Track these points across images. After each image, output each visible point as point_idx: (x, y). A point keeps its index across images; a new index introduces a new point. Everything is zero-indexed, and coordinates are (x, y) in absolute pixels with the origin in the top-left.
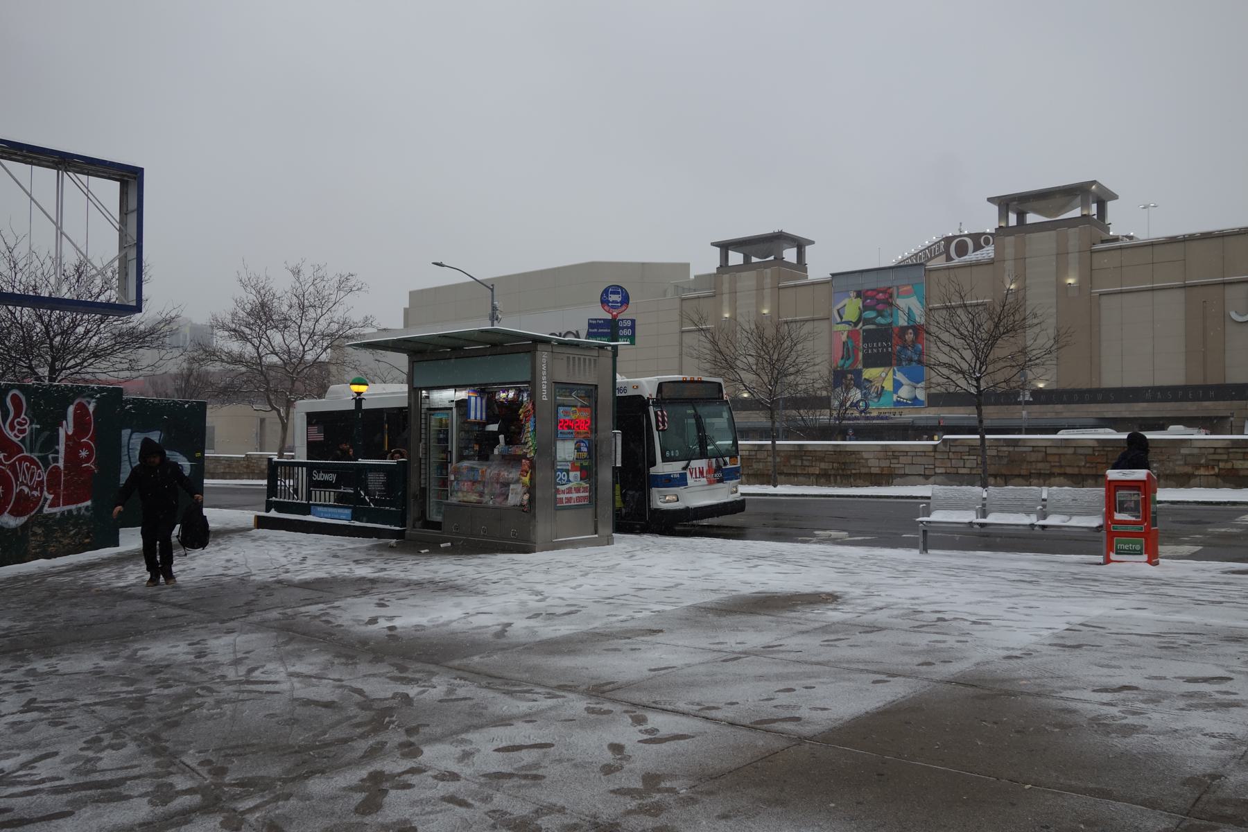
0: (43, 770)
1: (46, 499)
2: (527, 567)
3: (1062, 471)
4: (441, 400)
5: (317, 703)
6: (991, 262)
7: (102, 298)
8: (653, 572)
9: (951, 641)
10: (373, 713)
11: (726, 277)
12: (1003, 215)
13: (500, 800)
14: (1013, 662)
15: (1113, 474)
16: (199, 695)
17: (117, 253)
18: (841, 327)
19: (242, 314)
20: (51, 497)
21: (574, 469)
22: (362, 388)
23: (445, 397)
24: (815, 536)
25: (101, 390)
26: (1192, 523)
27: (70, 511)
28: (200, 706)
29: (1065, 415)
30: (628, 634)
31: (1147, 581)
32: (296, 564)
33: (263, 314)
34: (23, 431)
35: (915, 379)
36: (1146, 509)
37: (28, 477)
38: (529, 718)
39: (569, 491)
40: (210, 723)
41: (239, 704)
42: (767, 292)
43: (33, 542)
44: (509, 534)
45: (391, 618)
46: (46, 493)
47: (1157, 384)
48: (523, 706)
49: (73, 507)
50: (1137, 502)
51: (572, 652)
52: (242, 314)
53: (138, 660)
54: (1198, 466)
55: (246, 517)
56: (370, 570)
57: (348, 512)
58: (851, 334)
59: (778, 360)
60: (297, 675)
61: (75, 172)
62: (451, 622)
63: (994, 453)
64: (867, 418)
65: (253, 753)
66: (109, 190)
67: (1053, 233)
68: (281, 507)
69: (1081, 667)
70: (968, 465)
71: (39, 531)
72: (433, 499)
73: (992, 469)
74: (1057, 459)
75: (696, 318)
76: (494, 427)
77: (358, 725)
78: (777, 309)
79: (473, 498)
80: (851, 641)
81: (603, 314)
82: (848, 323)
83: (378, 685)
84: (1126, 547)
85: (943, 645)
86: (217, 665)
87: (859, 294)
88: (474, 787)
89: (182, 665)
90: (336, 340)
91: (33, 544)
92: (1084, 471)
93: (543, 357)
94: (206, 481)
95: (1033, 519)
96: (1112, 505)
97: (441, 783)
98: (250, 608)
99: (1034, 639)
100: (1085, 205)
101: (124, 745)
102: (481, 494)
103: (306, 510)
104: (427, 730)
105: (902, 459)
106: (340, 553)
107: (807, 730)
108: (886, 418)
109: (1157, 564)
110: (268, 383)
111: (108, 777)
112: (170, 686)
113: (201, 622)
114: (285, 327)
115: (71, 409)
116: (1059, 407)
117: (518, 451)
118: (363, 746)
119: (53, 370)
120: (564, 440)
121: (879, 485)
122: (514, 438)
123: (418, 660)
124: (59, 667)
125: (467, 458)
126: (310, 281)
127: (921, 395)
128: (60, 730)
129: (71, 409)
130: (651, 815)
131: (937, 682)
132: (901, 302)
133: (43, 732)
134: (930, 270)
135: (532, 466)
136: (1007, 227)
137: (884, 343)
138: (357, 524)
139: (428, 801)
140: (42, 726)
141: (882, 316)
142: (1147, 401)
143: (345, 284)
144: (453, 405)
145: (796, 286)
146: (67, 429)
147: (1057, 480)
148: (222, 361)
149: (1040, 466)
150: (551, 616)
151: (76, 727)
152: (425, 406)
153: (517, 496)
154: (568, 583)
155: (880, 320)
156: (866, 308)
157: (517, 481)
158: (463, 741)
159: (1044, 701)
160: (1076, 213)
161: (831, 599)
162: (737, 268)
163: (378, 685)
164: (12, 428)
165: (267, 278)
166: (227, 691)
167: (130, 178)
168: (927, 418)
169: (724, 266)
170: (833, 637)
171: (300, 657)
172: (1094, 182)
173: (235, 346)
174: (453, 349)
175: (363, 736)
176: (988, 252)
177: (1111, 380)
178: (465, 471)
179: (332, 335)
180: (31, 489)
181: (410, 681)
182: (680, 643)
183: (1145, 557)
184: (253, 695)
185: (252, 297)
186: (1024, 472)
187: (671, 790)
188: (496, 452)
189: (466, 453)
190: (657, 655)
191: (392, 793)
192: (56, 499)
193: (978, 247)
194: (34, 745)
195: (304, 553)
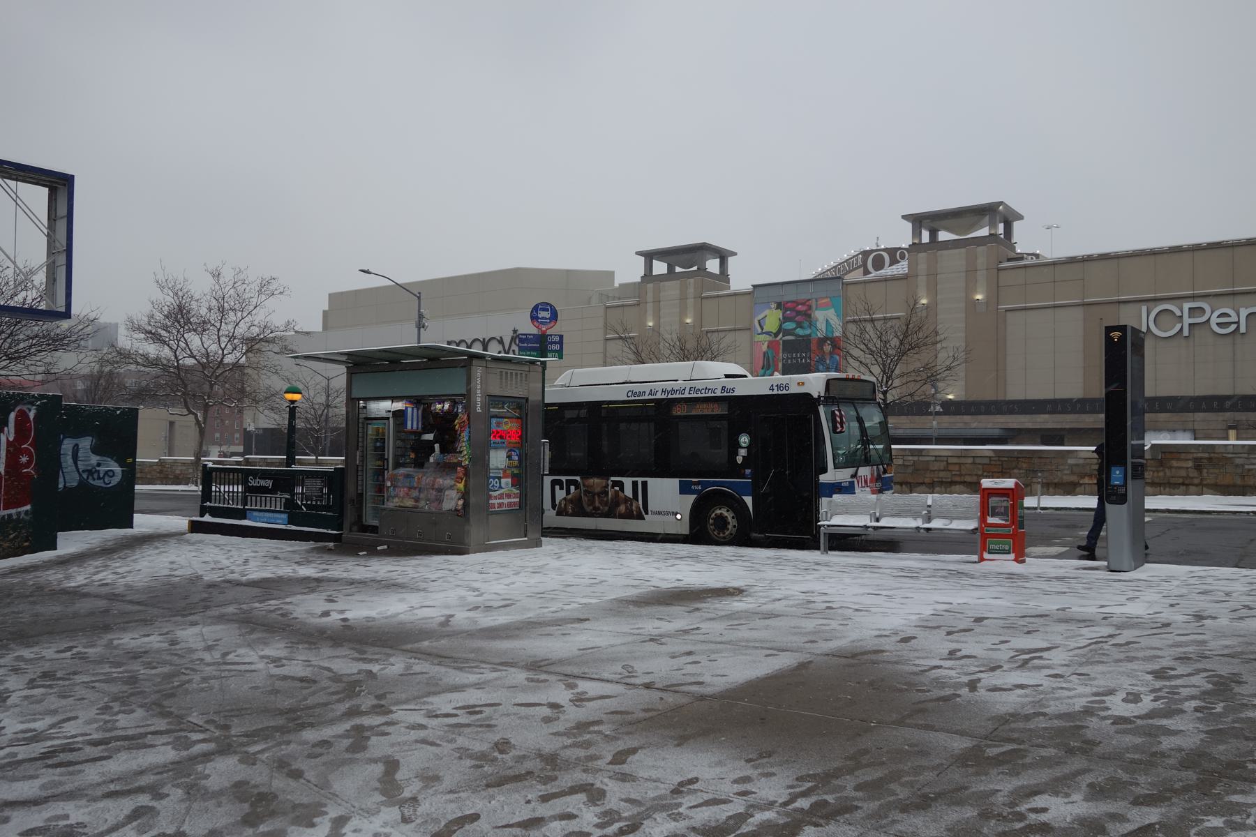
0: (71, 728)
2: (463, 567)
4: (379, 410)
5: (293, 678)
6: (905, 278)
8: (578, 571)
9: (834, 624)
11: (650, 286)
12: (917, 233)
13: (461, 741)
14: (882, 639)
15: (987, 483)
18: (762, 337)
19: (159, 316)
21: (505, 477)
22: (297, 397)
23: (382, 407)
25: (42, 397)
26: (1067, 527)
27: (10, 516)
28: (189, 681)
29: (974, 425)
30: (559, 622)
31: (1011, 576)
33: (181, 316)
38: (478, 686)
39: (501, 497)
40: (203, 694)
42: (690, 302)
44: (442, 537)
45: (342, 612)
47: (1058, 396)
48: (472, 678)
49: (13, 511)
50: (1006, 508)
51: (508, 637)
52: (159, 316)
53: (116, 648)
54: (1083, 476)
55: (180, 523)
57: (285, 516)
58: (771, 345)
60: (268, 657)
63: (900, 462)
66: (38, 196)
67: (963, 250)
68: (215, 512)
72: (369, 506)
74: (957, 468)
75: (620, 329)
76: (429, 437)
77: (333, 693)
78: (700, 318)
79: (409, 503)
80: (750, 626)
81: (529, 328)
82: (767, 333)
83: (345, 664)
86: (191, 651)
87: (779, 306)
89: (158, 651)
90: (252, 344)
93: (478, 371)
94: (137, 487)
95: (919, 523)
96: (985, 511)
98: (206, 605)
99: (904, 622)
100: (993, 225)
101: (133, 711)
102: (417, 500)
103: (242, 514)
104: (392, 696)
107: (708, 690)
109: (1024, 561)
110: (185, 386)
111: (130, 732)
115: (12, 416)
116: (967, 418)
117: (452, 459)
118: (342, 708)
120: (496, 448)
122: (449, 445)
123: (373, 645)
124: (44, 654)
125: (403, 465)
126: (231, 283)
129: (12, 416)
133: (53, 702)
134: (848, 284)
135: (467, 474)
136: (920, 243)
138: (294, 528)
139: (405, 743)
140: (53, 698)
141: (802, 327)
143: (265, 287)
144: (390, 415)
145: (718, 296)
147: (958, 487)
148: (138, 364)
149: (942, 474)
150: (489, 608)
152: (362, 416)
153: (452, 501)
155: (800, 331)
156: (786, 319)
157: (451, 488)
158: (424, 703)
159: (899, 667)
160: (984, 232)
161: (738, 592)
162: (661, 278)
163: (345, 664)
165: (185, 280)
166: (209, 670)
167: (59, 185)
169: (648, 275)
171: (266, 644)
172: (1001, 203)
173: (152, 349)
174: (391, 362)
175: (339, 701)
176: (902, 268)
177: (1016, 391)
181: (370, 661)
182: (605, 628)
183: (1012, 556)
186: (927, 480)
187: (599, 732)
188: (431, 460)
191: (374, 739)
193: (894, 262)
194: (54, 712)
195: (245, 556)
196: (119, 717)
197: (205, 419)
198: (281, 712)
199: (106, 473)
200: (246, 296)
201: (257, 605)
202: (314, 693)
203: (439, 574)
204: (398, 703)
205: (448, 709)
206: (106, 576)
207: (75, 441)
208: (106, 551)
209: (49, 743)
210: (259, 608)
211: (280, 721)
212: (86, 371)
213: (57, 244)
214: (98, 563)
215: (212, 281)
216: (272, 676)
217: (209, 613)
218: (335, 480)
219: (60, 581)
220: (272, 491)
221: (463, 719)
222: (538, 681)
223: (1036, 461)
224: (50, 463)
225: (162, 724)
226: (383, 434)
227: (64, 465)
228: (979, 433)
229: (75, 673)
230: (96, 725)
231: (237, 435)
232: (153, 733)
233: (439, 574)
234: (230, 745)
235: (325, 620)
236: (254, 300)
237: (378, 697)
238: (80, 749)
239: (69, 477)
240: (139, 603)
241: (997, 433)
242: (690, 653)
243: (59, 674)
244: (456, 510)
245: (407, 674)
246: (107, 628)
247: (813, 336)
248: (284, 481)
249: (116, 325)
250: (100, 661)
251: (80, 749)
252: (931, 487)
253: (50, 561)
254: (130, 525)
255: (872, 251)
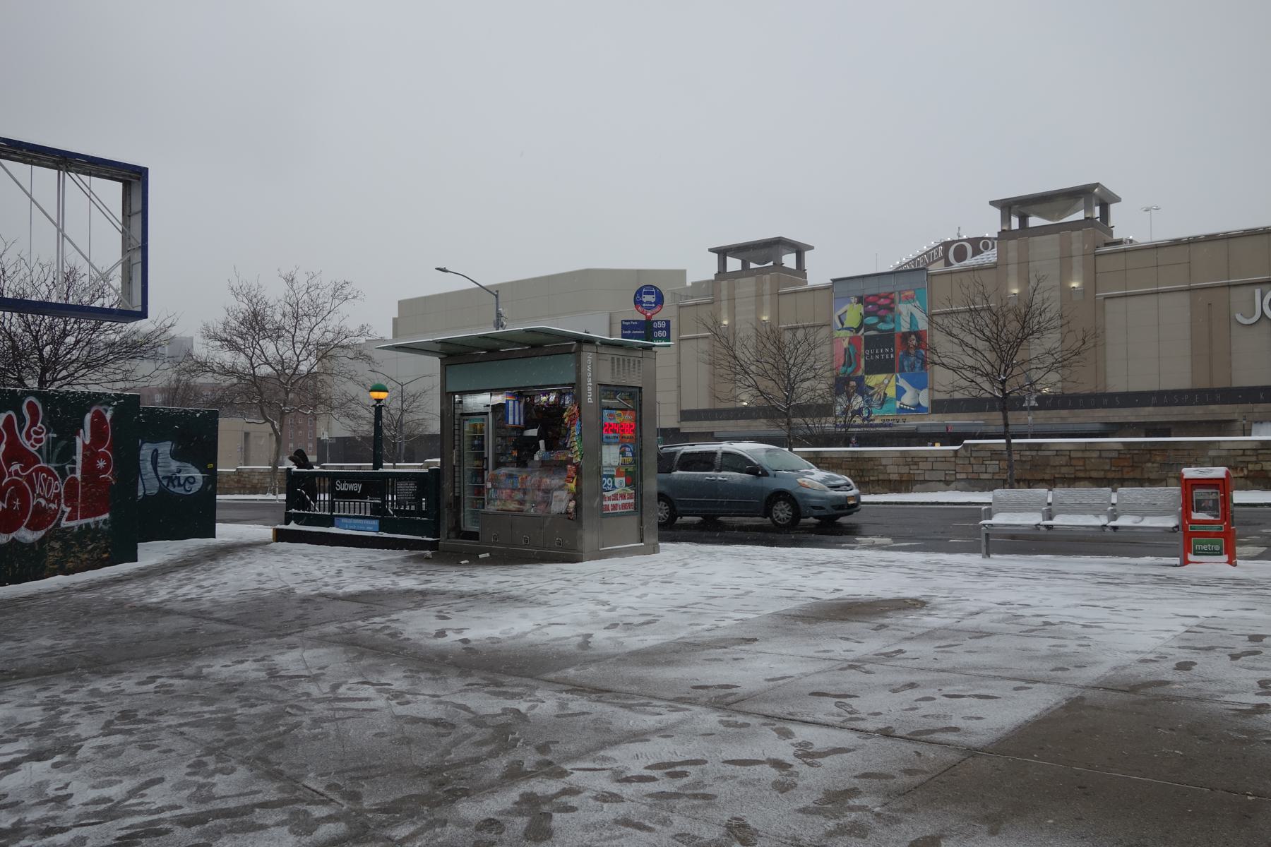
0: (156, 797)
1: (63, 512)
3: (1087, 475)
4: (476, 405)
5: (424, 720)
6: (994, 266)
7: (97, 304)
9: (1072, 646)
10: (491, 730)
12: (1006, 219)
15: (1190, 473)
16: (291, 714)
17: (119, 256)
18: (843, 333)
19: (234, 324)
20: (68, 510)
21: (619, 475)
22: (383, 395)
24: (857, 542)
25: (119, 397)
27: (88, 525)
29: (1071, 420)
30: (723, 643)
32: (332, 577)
34: (39, 441)
35: (919, 386)
36: (1225, 509)
37: (45, 489)
38: (664, 732)
39: (615, 497)
40: (317, 744)
41: (340, 722)
42: (767, 298)
43: (51, 558)
44: (556, 543)
45: (459, 631)
46: (63, 506)
47: (1163, 388)
48: (647, 721)
49: (91, 520)
50: (1215, 501)
51: (669, 663)
52: (234, 324)
53: (206, 678)
56: (414, 582)
57: (376, 523)
58: (852, 341)
59: (794, 365)
61: (77, 172)
62: (526, 633)
64: (872, 426)
65: (381, 775)
66: (111, 191)
68: (299, 519)
69: (1215, 668)
70: (990, 470)
71: (57, 545)
72: (467, 509)
73: (1017, 473)
76: (533, 432)
78: (776, 315)
79: (513, 506)
82: (849, 329)
84: (1204, 547)
85: (1066, 650)
87: (860, 300)
88: (645, 808)
89: (256, 682)
90: (325, 352)
91: (51, 559)
92: (1110, 475)
93: (588, 357)
95: (1103, 520)
96: (1188, 505)
97: (605, 805)
98: (303, 624)
99: (1159, 642)
100: (1088, 208)
101: (233, 770)
103: (329, 521)
105: (922, 465)
106: (375, 566)
107: (973, 741)
108: (890, 425)
110: (261, 395)
111: (232, 804)
112: (252, 706)
113: (258, 638)
114: (279, 337)
115: (88, 417)
116: (1064, 413)
117: (561, 456)
118: (499, 766)
119: (42, 382)
120: (608, 444)
121: (899, 491)
124: (123, 686)
126: (304, 289)
127: (925, 402)
128: (154, 753)
129: (88, 417)
130: (856, 836)
131: (1082, 687)
132: (903, 308)
133: (133, 756)
137: (886, 348)
138: (386, 535)
140: (132, 750)
142: (1155, 405)
143: (340, 292)
144: (489, 410)
145: (796, 292)
146: (83, 439)
148: (214, 372)
149: (1064, 470)
150: (628, 626)
151: (170, 751)
153: (561, 502)
154: (630, 592)
155: (882, 326)
156: (867, 314)
157: (561, 488)
160: (1079, 216)
162: (735, 274)
164: (29, 437)
166: (320, 709)
167: (134, 178)
168: (931, 425)
169: (722, 272)
170: (943, 643)
172: (1097, 185)
173: (227, 357)
174: (489, 351)
175: (493, 755)
177: (1117, 384)
178: (503, 478)
179: (328, 344)
180: (48, 501)
181: (513, 696)
182: (784, 651)
183: (1225, 558)
184: (350, 713)
185: (244, 307)
186: (1047, 477)
188: (536, 458)
189: (503, 459)
190: (765, 664)
192: (74, 510)
193: (977, 252)
194: (133, 771)
196: (217, 778)
197: (281, 426)
198: (424, 773)
199: (187, 479)
200: (320, 301)
201: (360, 623)
202: (455, 744)
203: (556, 585)
204: (570, 758)
205: (637, 769)
206: (190, 590)
207: (153, 446)
208: (187, 563)
209: (129, 821)
210: (366, 626)
211: (423, 787)
212: (164, 384)
213: (132, 241)
214: (181, 575)
215: (286, 286)
216: (398, 717)
217: (307, 633)
218: (427, 484)
219: (141, 596)
220: (361, 496)
221: (665, 786)
222: (736, 725)
223: (1172, 453)
224: (129, 468)
225: (271, 791)
226: (482, 431)
227: (143, 472)
228: (1077, 428)
229: (160, 713)
230: (186, 792)
231: (310, 445)
232: (264, 805)
233: (556, 585)
234: (365, 826)
235: (440, 641)
236: (328, 305)
237: (543, 749)
238: (167, 831)
239: (148, 485)
240: (227, 622)
241: (1097, 427)
242: (912, 685)
243: (141, 715)
244: (567, 513)
245: (564, 715)
246: (193, 653)
247: (897, 330)
248: (375, 485)
249: (192, 339)
250: (189, 697)
251: (167, 831)
252: (1051, 483)
253: (129, 574)
254: (212, 534)
255: (953, 242)
